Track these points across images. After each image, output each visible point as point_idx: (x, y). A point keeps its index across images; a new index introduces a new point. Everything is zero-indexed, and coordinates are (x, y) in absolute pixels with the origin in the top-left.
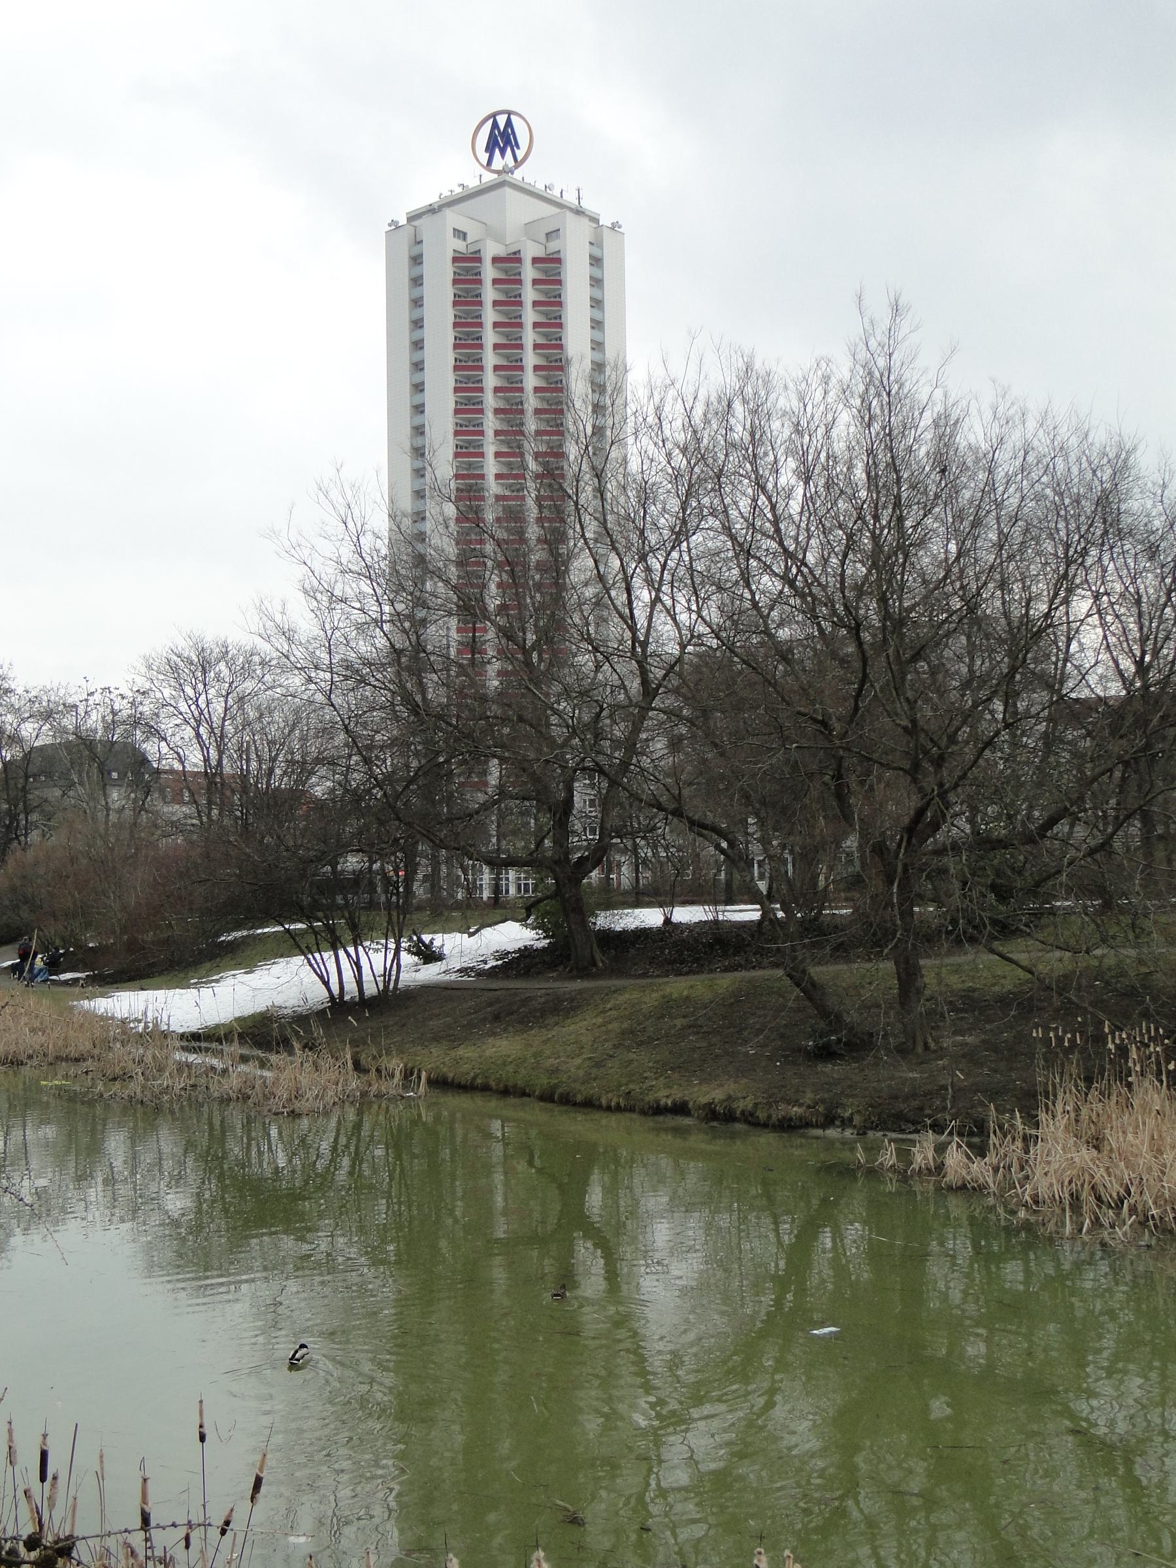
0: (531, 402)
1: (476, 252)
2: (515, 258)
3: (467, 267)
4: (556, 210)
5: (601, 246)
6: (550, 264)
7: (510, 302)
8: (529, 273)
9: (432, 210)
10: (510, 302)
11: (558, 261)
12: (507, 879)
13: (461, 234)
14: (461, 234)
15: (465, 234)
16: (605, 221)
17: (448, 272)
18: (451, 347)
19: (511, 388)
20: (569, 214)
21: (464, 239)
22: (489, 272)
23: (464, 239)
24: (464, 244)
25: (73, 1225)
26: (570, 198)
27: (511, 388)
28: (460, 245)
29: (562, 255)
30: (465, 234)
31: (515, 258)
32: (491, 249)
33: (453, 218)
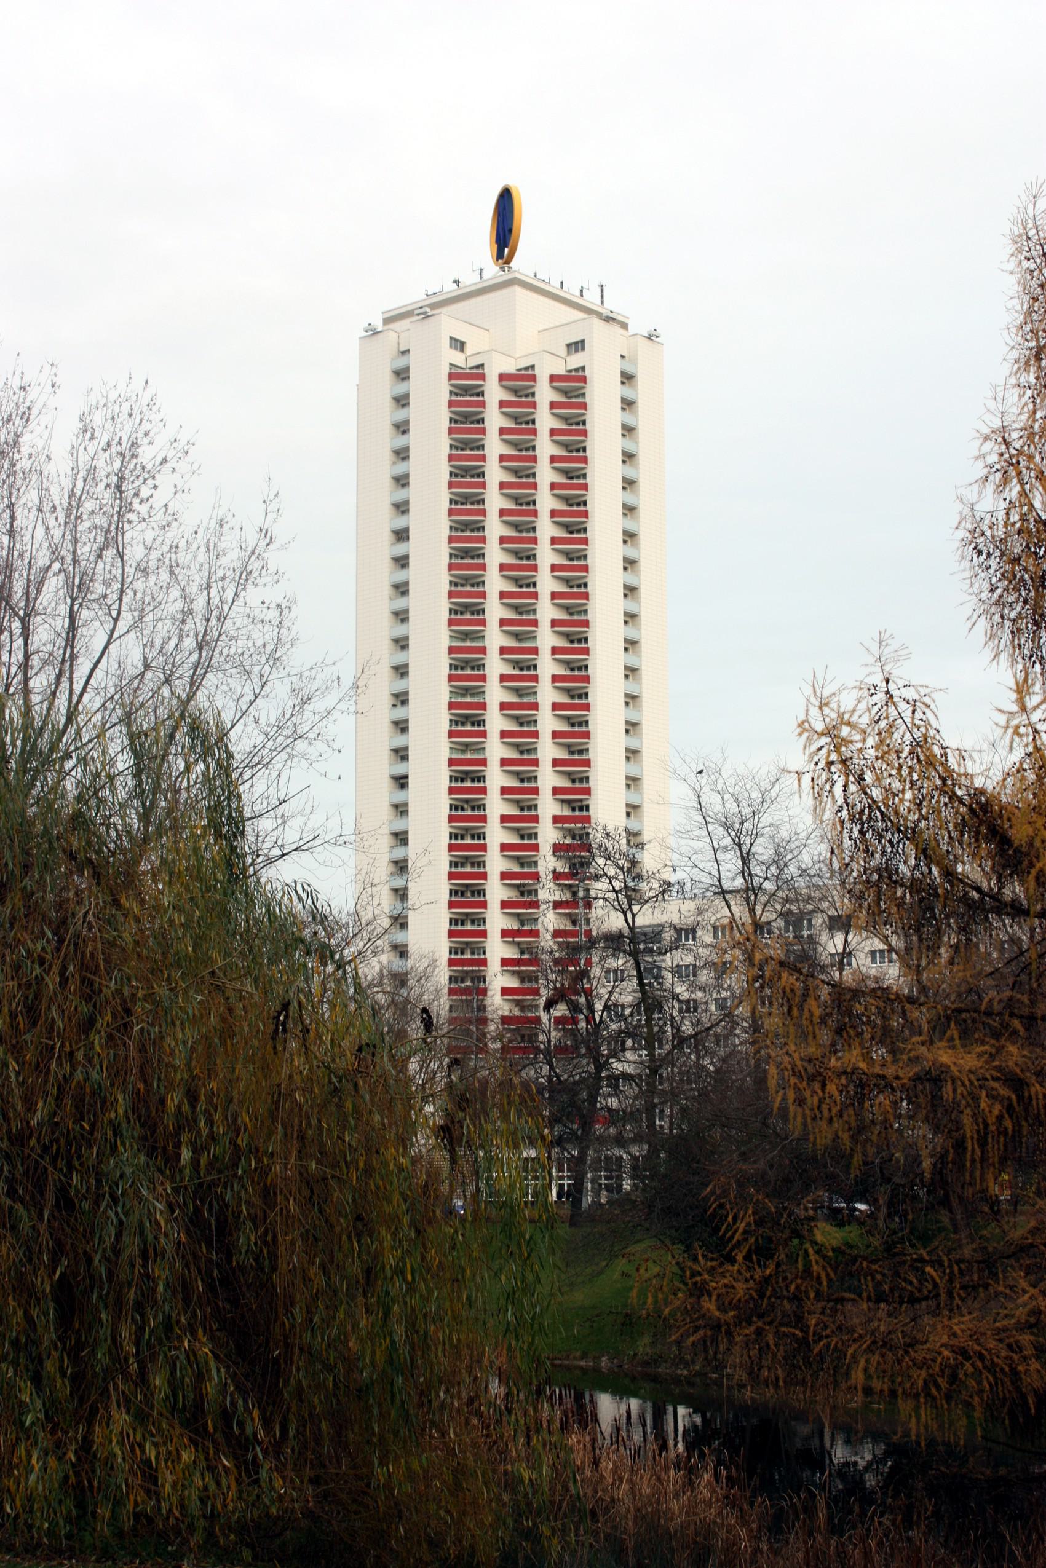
0: (548, 835)
1: (477, 367)
2: (528, 375)
3: (466, 388)
4: (580, 315)
5: (634, 361)
6: (572, 387)
7: (521, 428)
8: (545, 394)
9: (426, 311)
10: (521, 428)
11: (584, 379)
12: (469, 1529)
13: (459, 345)
14: (459, 345)
15: (463, 344)
16: (639, 325)
17: (443, 391)
18: (446, 485)
19: (522, 849)
20: (597, 322)
21: (462, 350)
22: (494, 393)
23: (462, 350)
24: (462, 356)
25: (978, 783)
26: (592, 298)
27: (522, 849)
28: (458, 359)
29: (587, 373)
30: (463, 344)
31: (528, 375)
32: (496, 367)
33: (448, 324)
